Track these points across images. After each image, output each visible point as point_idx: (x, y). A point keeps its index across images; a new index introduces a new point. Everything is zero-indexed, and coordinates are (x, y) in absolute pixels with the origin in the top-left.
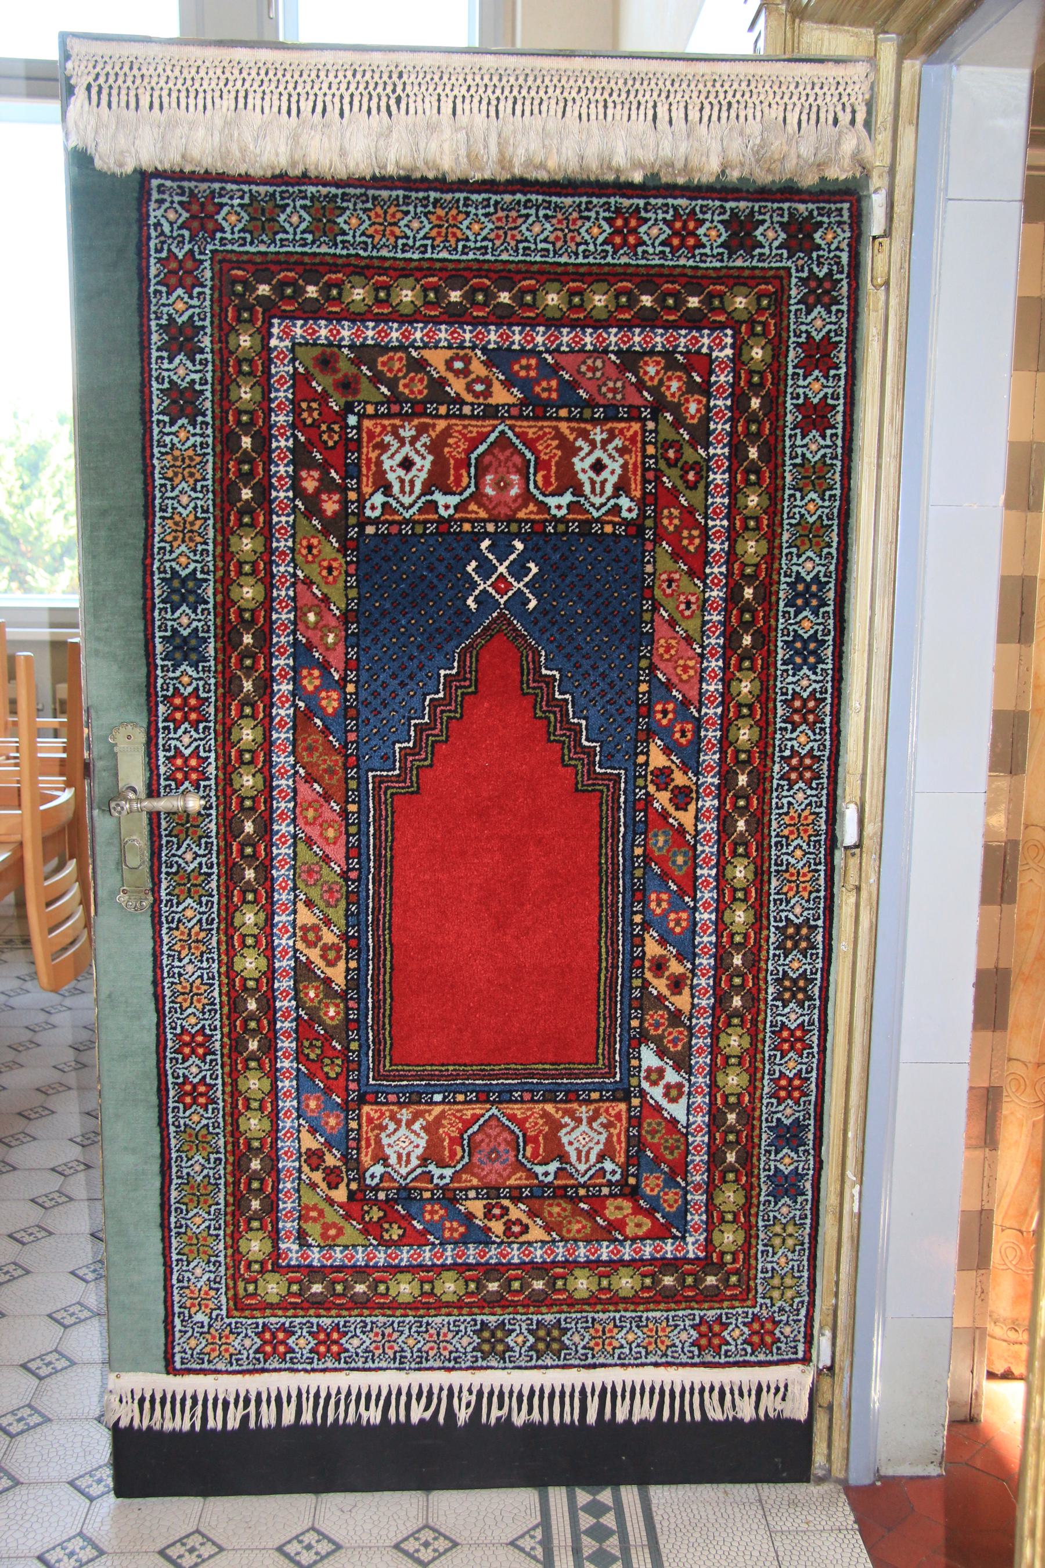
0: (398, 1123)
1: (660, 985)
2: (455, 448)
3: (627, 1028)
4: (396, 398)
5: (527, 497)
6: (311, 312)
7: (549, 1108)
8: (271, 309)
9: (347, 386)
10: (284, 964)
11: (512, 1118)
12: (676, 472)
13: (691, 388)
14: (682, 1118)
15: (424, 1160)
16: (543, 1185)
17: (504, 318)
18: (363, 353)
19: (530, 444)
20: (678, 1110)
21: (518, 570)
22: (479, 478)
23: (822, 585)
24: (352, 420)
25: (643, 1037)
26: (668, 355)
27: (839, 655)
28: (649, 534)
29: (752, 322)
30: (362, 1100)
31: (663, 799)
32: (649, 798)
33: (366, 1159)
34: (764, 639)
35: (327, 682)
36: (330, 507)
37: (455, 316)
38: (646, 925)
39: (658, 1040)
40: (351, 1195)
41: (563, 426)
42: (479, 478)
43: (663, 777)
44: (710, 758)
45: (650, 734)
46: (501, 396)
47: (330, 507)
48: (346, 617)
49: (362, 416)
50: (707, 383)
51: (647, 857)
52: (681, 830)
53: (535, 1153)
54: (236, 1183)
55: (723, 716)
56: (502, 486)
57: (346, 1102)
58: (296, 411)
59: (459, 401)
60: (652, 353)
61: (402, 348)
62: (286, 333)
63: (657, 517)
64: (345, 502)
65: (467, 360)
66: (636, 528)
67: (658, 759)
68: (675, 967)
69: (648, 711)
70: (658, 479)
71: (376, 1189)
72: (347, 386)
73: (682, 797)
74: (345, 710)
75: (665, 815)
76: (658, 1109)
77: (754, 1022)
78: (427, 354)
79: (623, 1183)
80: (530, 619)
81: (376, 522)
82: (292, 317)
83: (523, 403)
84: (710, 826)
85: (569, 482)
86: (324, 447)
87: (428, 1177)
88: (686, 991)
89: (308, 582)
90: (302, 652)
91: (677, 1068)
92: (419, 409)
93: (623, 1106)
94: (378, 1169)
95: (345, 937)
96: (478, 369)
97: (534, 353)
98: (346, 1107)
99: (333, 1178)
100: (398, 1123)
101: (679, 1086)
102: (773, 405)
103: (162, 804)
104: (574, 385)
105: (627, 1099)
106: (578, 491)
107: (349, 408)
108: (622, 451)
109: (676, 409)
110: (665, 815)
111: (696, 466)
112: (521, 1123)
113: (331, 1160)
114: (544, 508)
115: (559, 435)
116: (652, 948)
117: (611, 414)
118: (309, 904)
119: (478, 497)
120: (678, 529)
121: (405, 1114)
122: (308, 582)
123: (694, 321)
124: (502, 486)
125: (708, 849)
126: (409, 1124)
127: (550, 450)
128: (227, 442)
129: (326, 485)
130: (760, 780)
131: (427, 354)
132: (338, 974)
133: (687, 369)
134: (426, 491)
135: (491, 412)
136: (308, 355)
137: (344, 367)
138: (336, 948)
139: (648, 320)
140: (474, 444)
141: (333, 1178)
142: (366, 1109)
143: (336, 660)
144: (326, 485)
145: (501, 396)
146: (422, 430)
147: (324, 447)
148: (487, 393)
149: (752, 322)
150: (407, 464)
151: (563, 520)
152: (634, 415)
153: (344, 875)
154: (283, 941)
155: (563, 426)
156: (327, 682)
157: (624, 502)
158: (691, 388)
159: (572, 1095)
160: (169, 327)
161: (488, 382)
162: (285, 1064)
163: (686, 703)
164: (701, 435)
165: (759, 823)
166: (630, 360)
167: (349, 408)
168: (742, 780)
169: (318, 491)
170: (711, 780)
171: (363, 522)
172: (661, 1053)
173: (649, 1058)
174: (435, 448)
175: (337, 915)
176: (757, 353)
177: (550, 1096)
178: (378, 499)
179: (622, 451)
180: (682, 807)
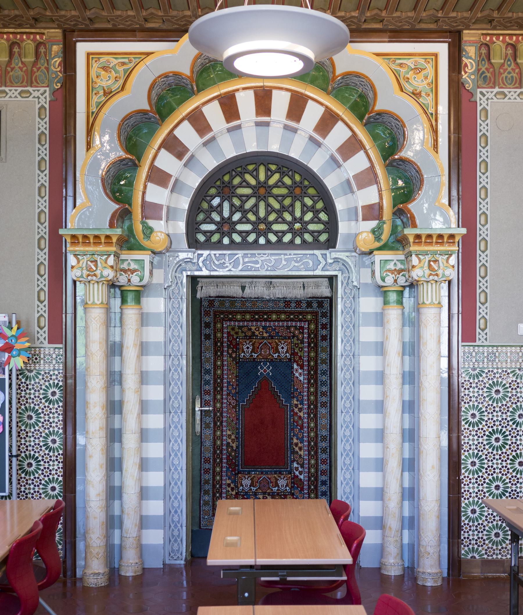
0: (245, 478)
1: (297, 449)
2: (257, 345)
3: (291, 458)
4: (246, 336)
5: (270, 354)
6: (230, 320)
7: (275, 475)
8: (223, 319)
9: (237, 333)
10: (224, 443)
11: (268, 477)
12: (298, 349)
13: (300, 333)
14: (302, 415)
15: (250, 486)
16: (274, 492)
17: (266, 320)
18: (240, 327)
19: (270, 344)
20: (302, 477)
21: (268, 368)
22: (261, 350)
23: (327, 460)
24: (238, 340)
25: (294, 461)
26: (295, 327)
27: (330, 462)
28: (292, 361)
29: (311, 321)
30: (239, 473)
31: (296, 410)
32: (293, 410)
33: (239, 485)
34: (316, 381)
35: (233, 388)
36: (234, 355)
37: (257, 320)
38: (294, 436)
39: (297, 461)
40: (236, 493)
41: (276, 340)
42: (261, 350)
43: (296, 406)
44: (306, 368)
45: (293, 397)
46: (265, 335)
47: (234, 355)
48: (236, 377)
49: (239, 339)
50: (303, 332)
51: (294, 421)
52: (300, 417)
53: (273, 485)
54: (226, 312)
55: (308, 360)
56: (265, 352)
57: (235, 473)
58: (228, 338)
59: (257, 336)
60: (293, 326)
61: (247, 326)
62: (226, 324)
63: (294, 358)
64: (236, 355)
65: (259, 328)
66: (290, 360)
67: (296, 402)
68: (300, 445)
69: (293, 393)
70: (294, 350)
71: (241, 492)
72: (237, 333)
73: (300, 410)
74: (236, 393)
75: (297, 413)
76: (297, 452)
77: (316, 349)
78: (252, 327)
79: (291, 492)
80: (271, 377)
81: (242, 359)
82: (227, 321)
83: (269, 336)
84: (306, 416)
85: (277, 351)
86: (233, 345)
87: (251, 489)
88: (303, 451)
89: (230, 370)
90: (228, 383)
91: (301, 467)
92: (250, 338)
93: (290, 475)
94: (241, 488)
95: (235, 437)
96: (261, 330)
97: (271, 327)
98: (236, 474)
99: (233, 489)
100: (245, 478)
101: (302, 471)
102: (316, 336)
103: (202, 409)
104: (278, 333)
105: (291, 474)
106: (279, 353)
107: (237, 338)
108: (287, 345)
109: (297, 337)
110: (297, 413)
111: (302, 348)
112: (270, 479)
113: (232, 485)
114: (273, 356)
115: (276, 342)
116: (295, 441)
117: (285, 338)
118: (229, 430)
119: (261, 354)
120: (298, 396)
121: (247, 477)
122: (230, 370)
123: (300, 320)
124: (265, 352)
125: (306, 420)
126: (247, 478)
127: (274, 345)
128: (215, 344)
129: (233, 352)
130: (316, 407)
131: (252, 327)
132: (234, 445)
133: (299, 329)
134: (251, 353)
135: (263, 338)
136: (230, 328)
137: (237, 330)
138: (234, 439)
139: (292, 320)
140: (260, 344)
141: (233, 489)
142: (239, 475)
143: (235, 384)
144: (233, 352)
145: (265, 335)
146: (250, 342)
147: (233, 345)
148: (263, 334)
149: (311, 321)
150: (248, 348)
151: (276, 359)
152: (289, 338)
153: (236, 424)
154: (224, 438)
155: (276, 340)
156: (233, 388)
157: (288, 355)
158: (300, 333)
159: (280, 473)
160: (205, 335)
161: (262, 332)
162: (224, 465)
163: (300, 392)
164: (302, 342)
165: (316, 416)
166: (288, 327)
167: (237, 338)
168: (312, 381)
169: (232, 353)
170: (306, 407)
171: (240, 358)
172: (298, 464)
173: (295, 465)
174: (253, 345)
175: (234, 432)
176: (312, 398)
177: (275, 473)
178: (243, 354)
179: (287, 345)
180: (300, 412)
